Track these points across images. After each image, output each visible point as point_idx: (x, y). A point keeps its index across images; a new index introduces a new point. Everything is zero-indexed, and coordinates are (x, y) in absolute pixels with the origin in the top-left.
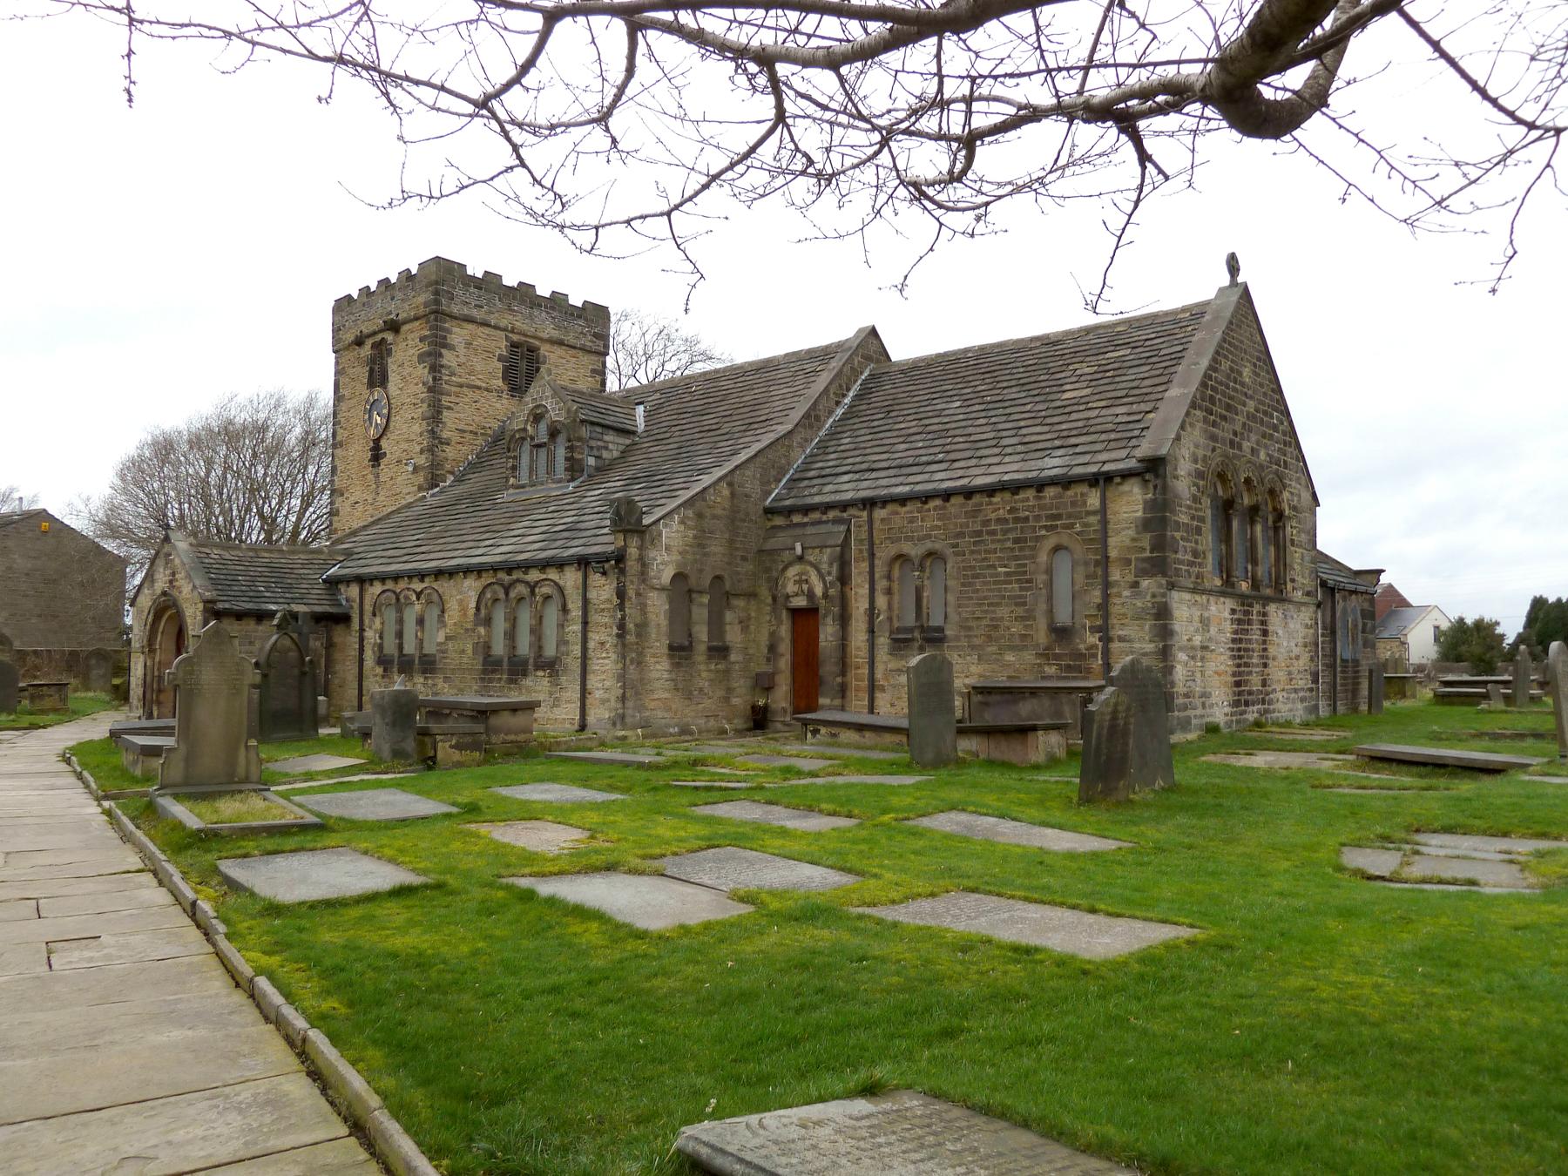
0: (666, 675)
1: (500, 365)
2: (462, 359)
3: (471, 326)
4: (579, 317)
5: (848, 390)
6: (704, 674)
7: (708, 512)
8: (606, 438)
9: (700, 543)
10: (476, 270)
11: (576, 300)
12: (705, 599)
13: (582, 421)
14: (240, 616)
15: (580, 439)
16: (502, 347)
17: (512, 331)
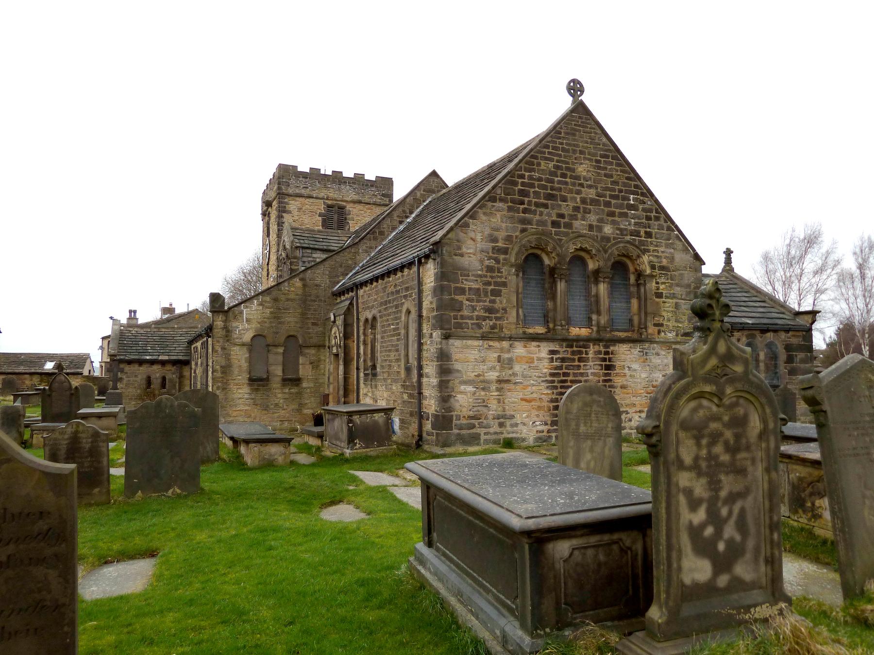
0: (246, 396)
1: (320, 218)
2: (296, 218)
3: (301, 199)
4: (372, 186)
5: (411, 213)
6: (279, 395)
7: (283, 298)
8: (314, 255)
9: (276, 316)
10: (304, 168)
11: (370, 176)
12: (281, 350)
13: (297, 247)
14: (130, 362)
15: (295, 258)
16: (322, 208)
17: (327, 199)
